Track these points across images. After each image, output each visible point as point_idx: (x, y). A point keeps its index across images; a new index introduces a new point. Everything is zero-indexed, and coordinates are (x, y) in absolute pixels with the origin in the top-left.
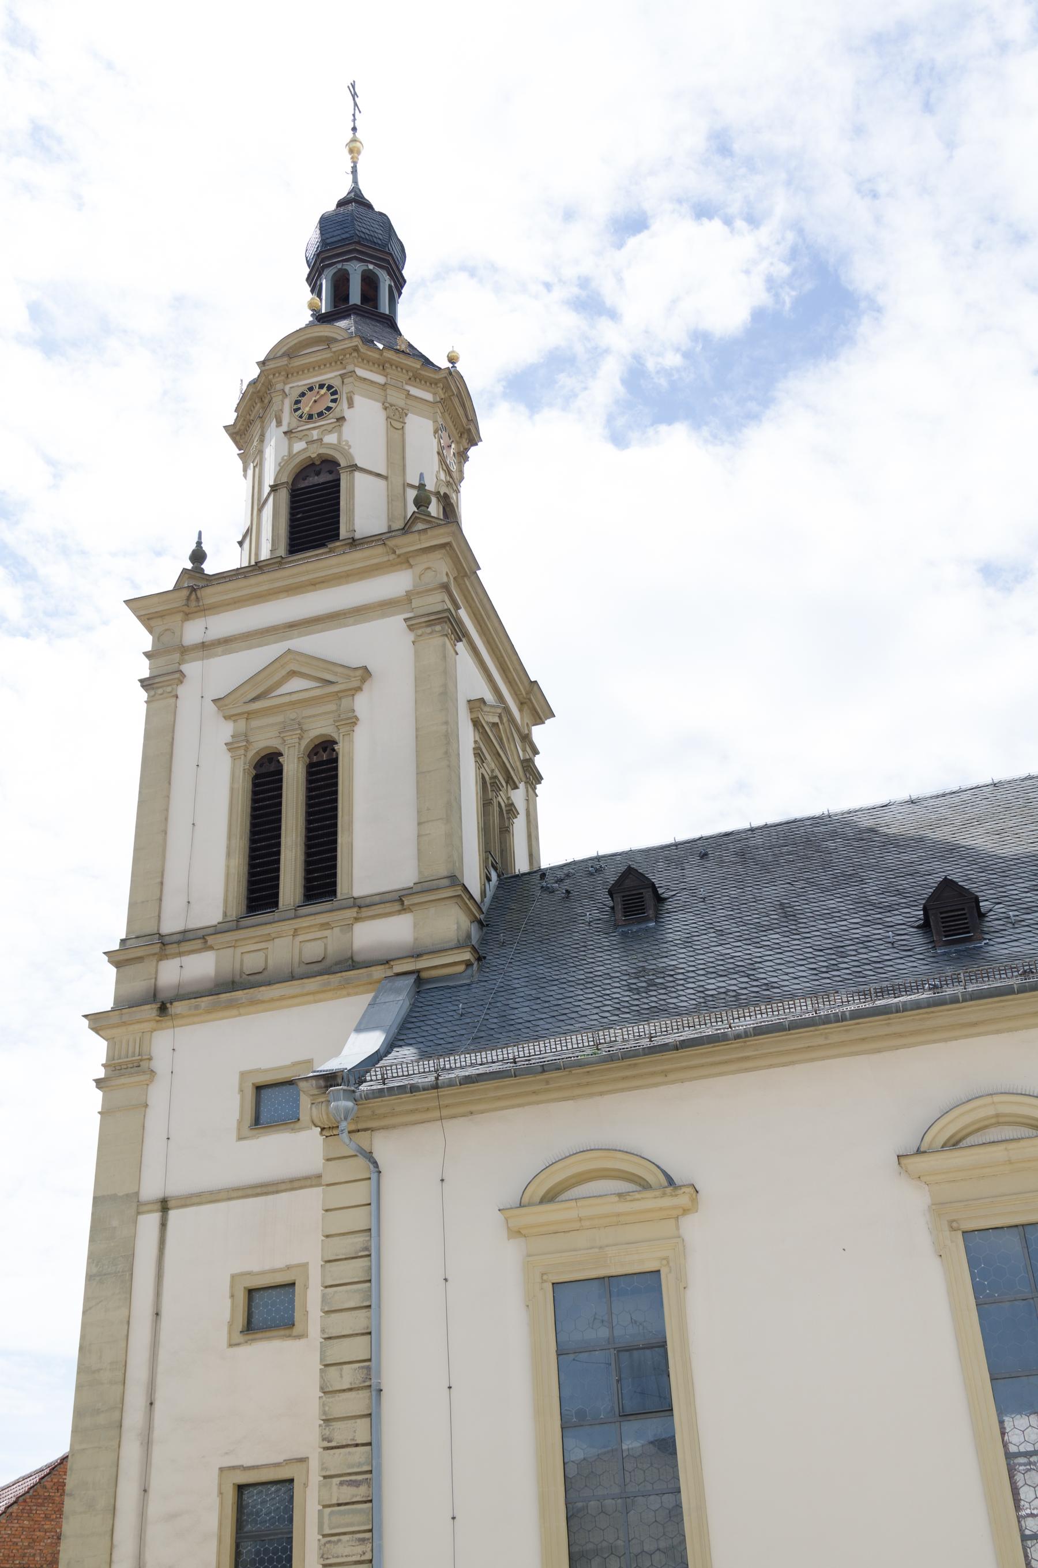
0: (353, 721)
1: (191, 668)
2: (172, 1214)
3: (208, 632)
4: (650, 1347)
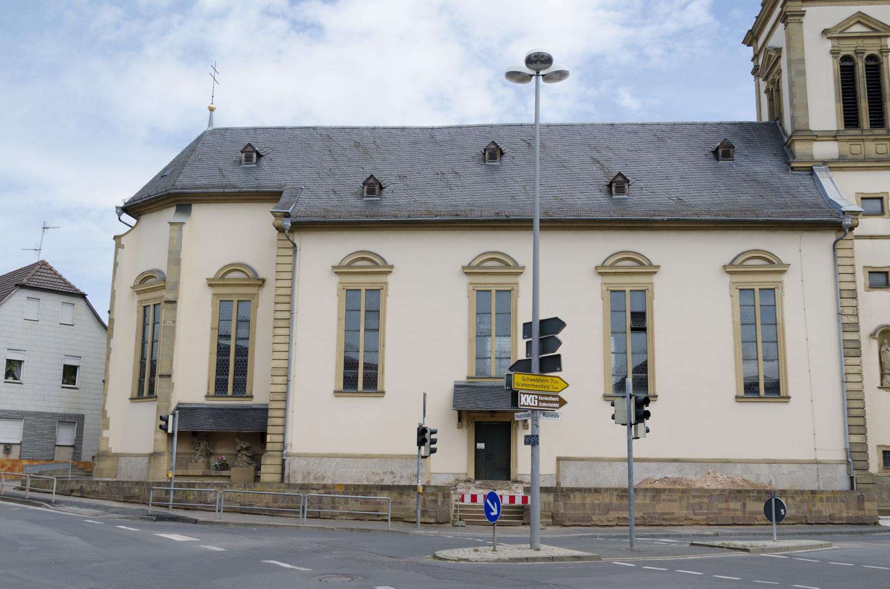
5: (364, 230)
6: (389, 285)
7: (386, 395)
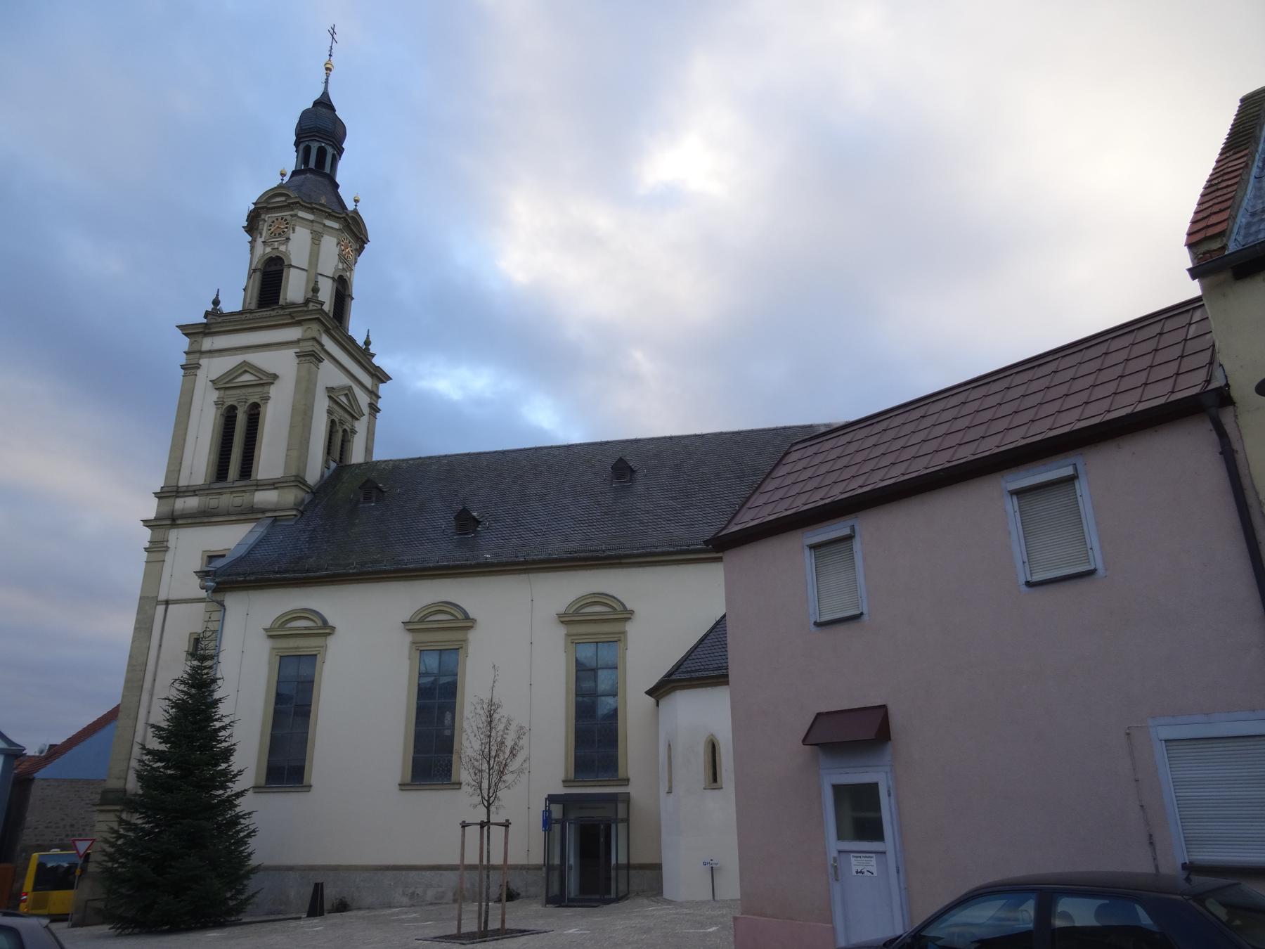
0: (268, 398)
1: (204, 362)
2: (170, 606)
3: (214, 345)
5: (393, 581)
6: (628, 635)
7: (312, 789)
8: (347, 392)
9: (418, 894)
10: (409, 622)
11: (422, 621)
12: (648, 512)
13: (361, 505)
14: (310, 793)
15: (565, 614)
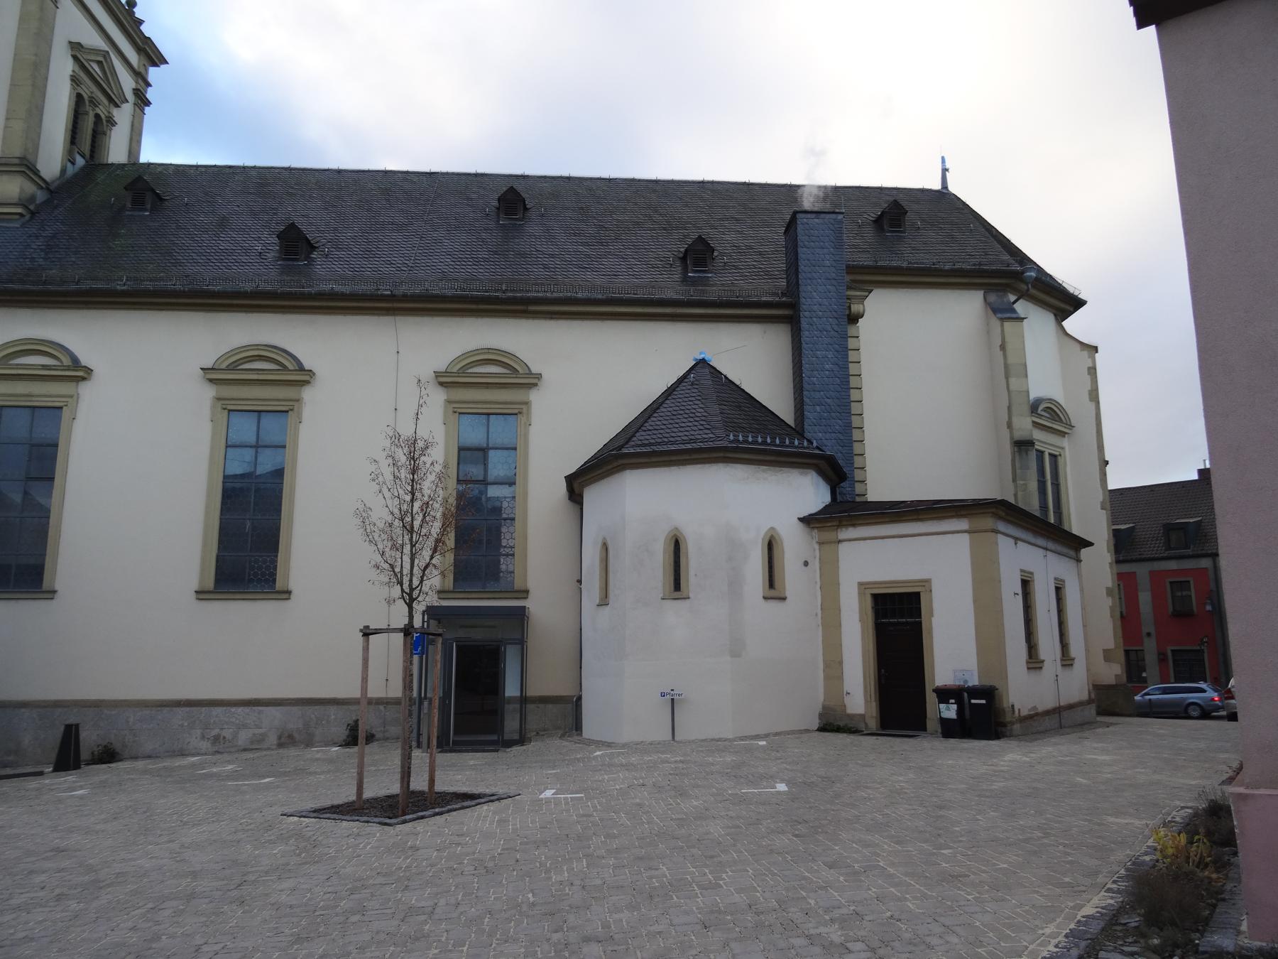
4: (49, 445)
8: (101, 59)
9: (224, 738)
10: (212, 369)
11: (233, 367)
12: (552, 256)
13: (127, 213)
14: (54, 601)
15: (446, 372)
